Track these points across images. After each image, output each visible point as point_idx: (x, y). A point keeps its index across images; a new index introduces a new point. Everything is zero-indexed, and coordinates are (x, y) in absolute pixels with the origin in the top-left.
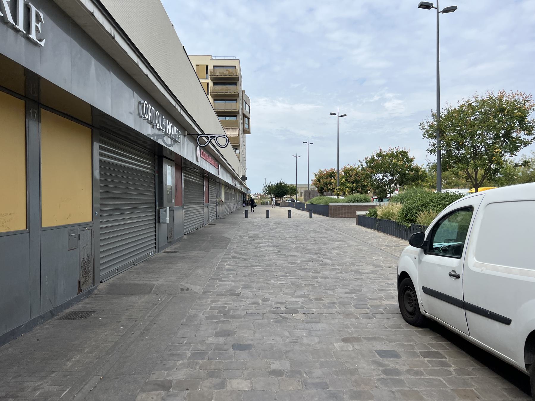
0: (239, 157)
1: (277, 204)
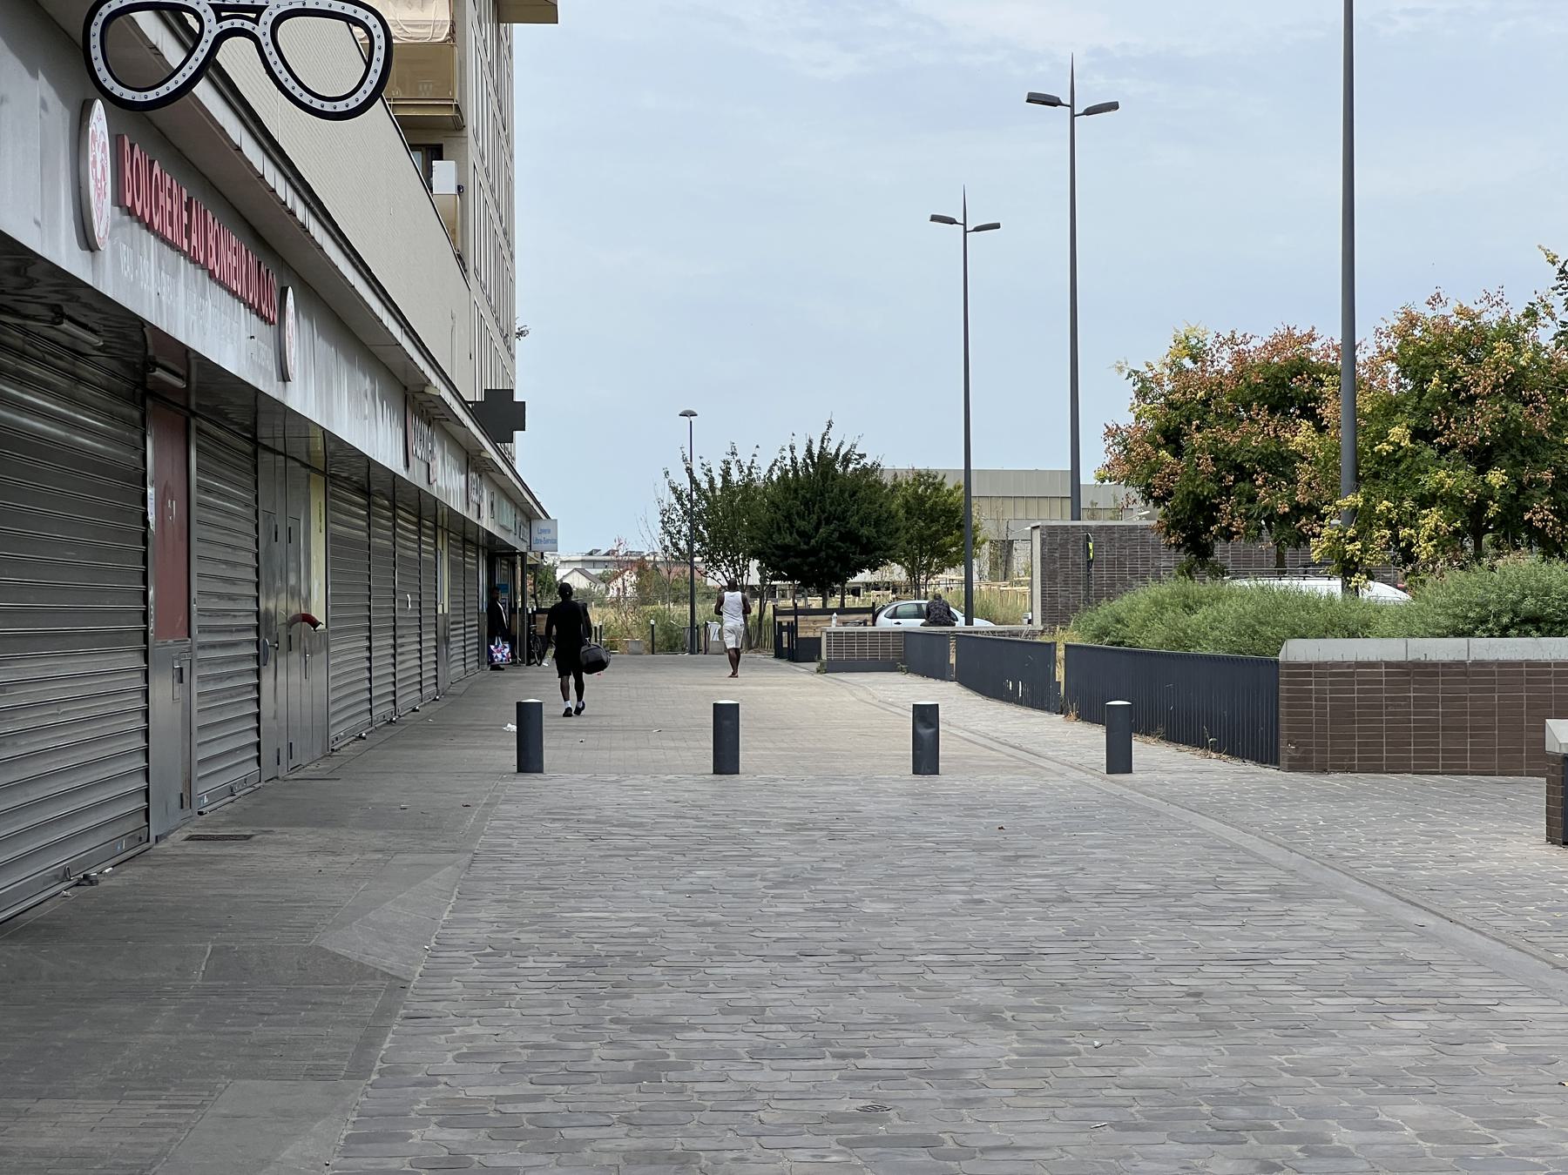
0: (454, 229)
1: (796, 650)
